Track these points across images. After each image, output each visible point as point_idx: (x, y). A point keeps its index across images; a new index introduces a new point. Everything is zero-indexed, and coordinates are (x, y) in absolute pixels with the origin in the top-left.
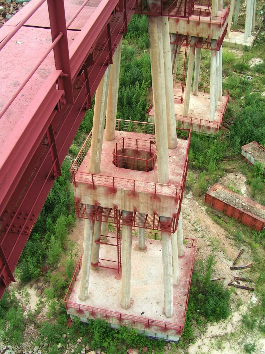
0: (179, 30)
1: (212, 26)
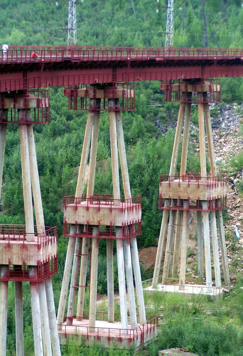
0: (78, 219)
1: (113, 212)
